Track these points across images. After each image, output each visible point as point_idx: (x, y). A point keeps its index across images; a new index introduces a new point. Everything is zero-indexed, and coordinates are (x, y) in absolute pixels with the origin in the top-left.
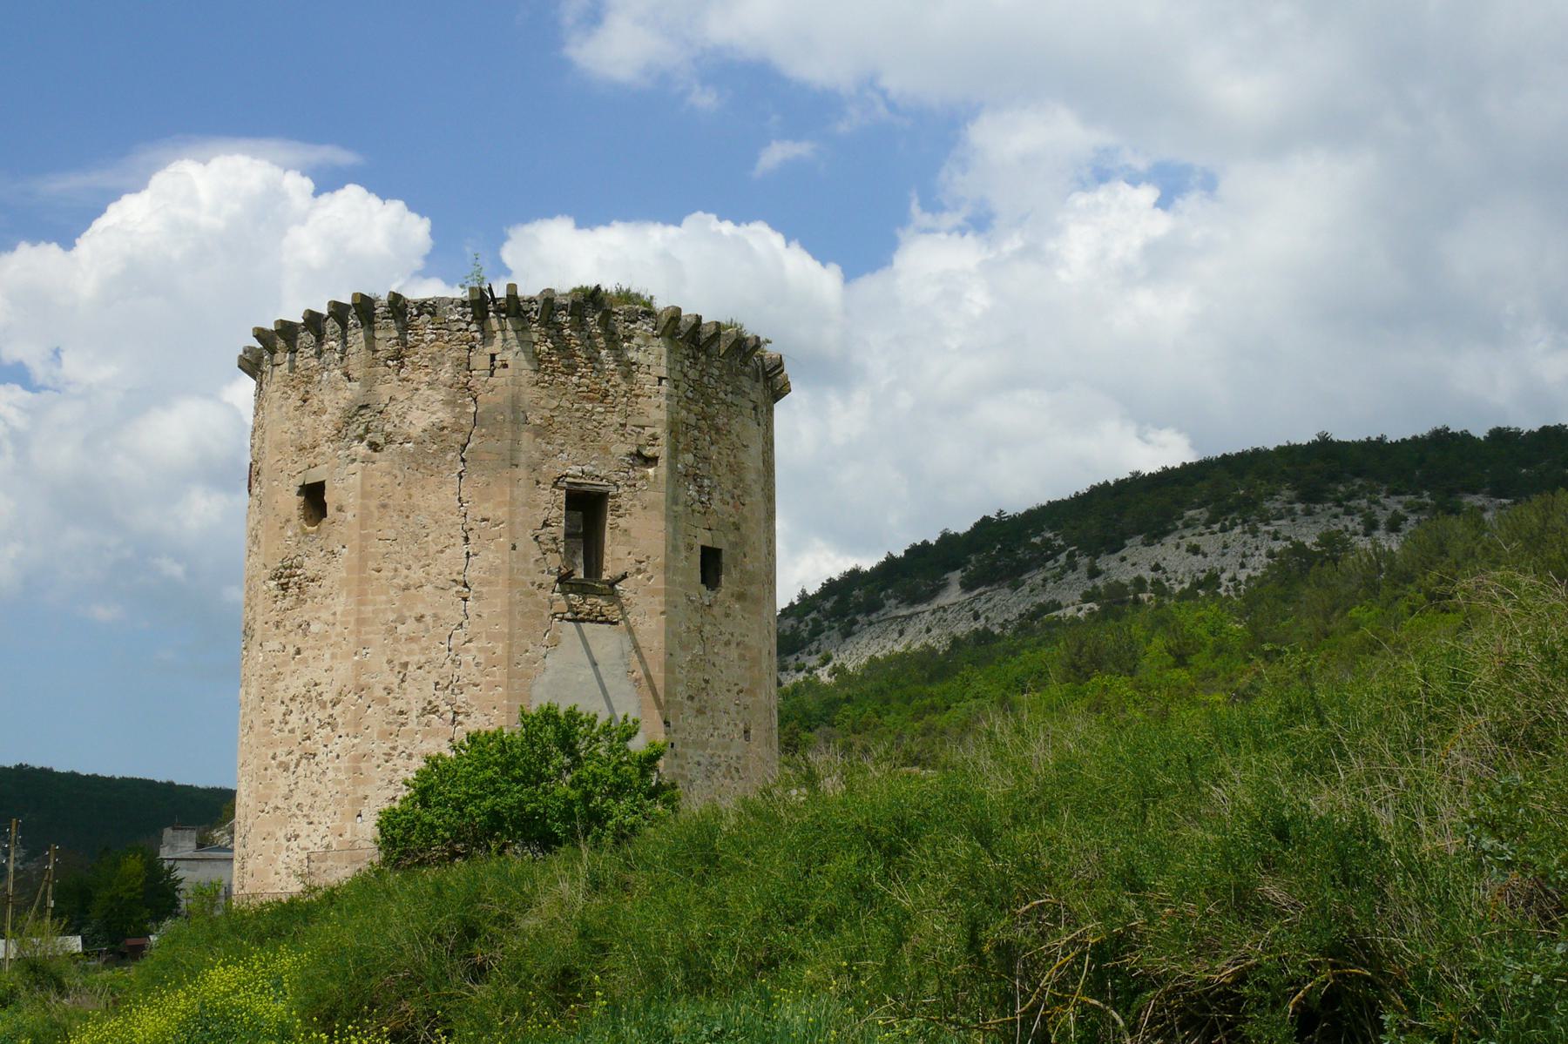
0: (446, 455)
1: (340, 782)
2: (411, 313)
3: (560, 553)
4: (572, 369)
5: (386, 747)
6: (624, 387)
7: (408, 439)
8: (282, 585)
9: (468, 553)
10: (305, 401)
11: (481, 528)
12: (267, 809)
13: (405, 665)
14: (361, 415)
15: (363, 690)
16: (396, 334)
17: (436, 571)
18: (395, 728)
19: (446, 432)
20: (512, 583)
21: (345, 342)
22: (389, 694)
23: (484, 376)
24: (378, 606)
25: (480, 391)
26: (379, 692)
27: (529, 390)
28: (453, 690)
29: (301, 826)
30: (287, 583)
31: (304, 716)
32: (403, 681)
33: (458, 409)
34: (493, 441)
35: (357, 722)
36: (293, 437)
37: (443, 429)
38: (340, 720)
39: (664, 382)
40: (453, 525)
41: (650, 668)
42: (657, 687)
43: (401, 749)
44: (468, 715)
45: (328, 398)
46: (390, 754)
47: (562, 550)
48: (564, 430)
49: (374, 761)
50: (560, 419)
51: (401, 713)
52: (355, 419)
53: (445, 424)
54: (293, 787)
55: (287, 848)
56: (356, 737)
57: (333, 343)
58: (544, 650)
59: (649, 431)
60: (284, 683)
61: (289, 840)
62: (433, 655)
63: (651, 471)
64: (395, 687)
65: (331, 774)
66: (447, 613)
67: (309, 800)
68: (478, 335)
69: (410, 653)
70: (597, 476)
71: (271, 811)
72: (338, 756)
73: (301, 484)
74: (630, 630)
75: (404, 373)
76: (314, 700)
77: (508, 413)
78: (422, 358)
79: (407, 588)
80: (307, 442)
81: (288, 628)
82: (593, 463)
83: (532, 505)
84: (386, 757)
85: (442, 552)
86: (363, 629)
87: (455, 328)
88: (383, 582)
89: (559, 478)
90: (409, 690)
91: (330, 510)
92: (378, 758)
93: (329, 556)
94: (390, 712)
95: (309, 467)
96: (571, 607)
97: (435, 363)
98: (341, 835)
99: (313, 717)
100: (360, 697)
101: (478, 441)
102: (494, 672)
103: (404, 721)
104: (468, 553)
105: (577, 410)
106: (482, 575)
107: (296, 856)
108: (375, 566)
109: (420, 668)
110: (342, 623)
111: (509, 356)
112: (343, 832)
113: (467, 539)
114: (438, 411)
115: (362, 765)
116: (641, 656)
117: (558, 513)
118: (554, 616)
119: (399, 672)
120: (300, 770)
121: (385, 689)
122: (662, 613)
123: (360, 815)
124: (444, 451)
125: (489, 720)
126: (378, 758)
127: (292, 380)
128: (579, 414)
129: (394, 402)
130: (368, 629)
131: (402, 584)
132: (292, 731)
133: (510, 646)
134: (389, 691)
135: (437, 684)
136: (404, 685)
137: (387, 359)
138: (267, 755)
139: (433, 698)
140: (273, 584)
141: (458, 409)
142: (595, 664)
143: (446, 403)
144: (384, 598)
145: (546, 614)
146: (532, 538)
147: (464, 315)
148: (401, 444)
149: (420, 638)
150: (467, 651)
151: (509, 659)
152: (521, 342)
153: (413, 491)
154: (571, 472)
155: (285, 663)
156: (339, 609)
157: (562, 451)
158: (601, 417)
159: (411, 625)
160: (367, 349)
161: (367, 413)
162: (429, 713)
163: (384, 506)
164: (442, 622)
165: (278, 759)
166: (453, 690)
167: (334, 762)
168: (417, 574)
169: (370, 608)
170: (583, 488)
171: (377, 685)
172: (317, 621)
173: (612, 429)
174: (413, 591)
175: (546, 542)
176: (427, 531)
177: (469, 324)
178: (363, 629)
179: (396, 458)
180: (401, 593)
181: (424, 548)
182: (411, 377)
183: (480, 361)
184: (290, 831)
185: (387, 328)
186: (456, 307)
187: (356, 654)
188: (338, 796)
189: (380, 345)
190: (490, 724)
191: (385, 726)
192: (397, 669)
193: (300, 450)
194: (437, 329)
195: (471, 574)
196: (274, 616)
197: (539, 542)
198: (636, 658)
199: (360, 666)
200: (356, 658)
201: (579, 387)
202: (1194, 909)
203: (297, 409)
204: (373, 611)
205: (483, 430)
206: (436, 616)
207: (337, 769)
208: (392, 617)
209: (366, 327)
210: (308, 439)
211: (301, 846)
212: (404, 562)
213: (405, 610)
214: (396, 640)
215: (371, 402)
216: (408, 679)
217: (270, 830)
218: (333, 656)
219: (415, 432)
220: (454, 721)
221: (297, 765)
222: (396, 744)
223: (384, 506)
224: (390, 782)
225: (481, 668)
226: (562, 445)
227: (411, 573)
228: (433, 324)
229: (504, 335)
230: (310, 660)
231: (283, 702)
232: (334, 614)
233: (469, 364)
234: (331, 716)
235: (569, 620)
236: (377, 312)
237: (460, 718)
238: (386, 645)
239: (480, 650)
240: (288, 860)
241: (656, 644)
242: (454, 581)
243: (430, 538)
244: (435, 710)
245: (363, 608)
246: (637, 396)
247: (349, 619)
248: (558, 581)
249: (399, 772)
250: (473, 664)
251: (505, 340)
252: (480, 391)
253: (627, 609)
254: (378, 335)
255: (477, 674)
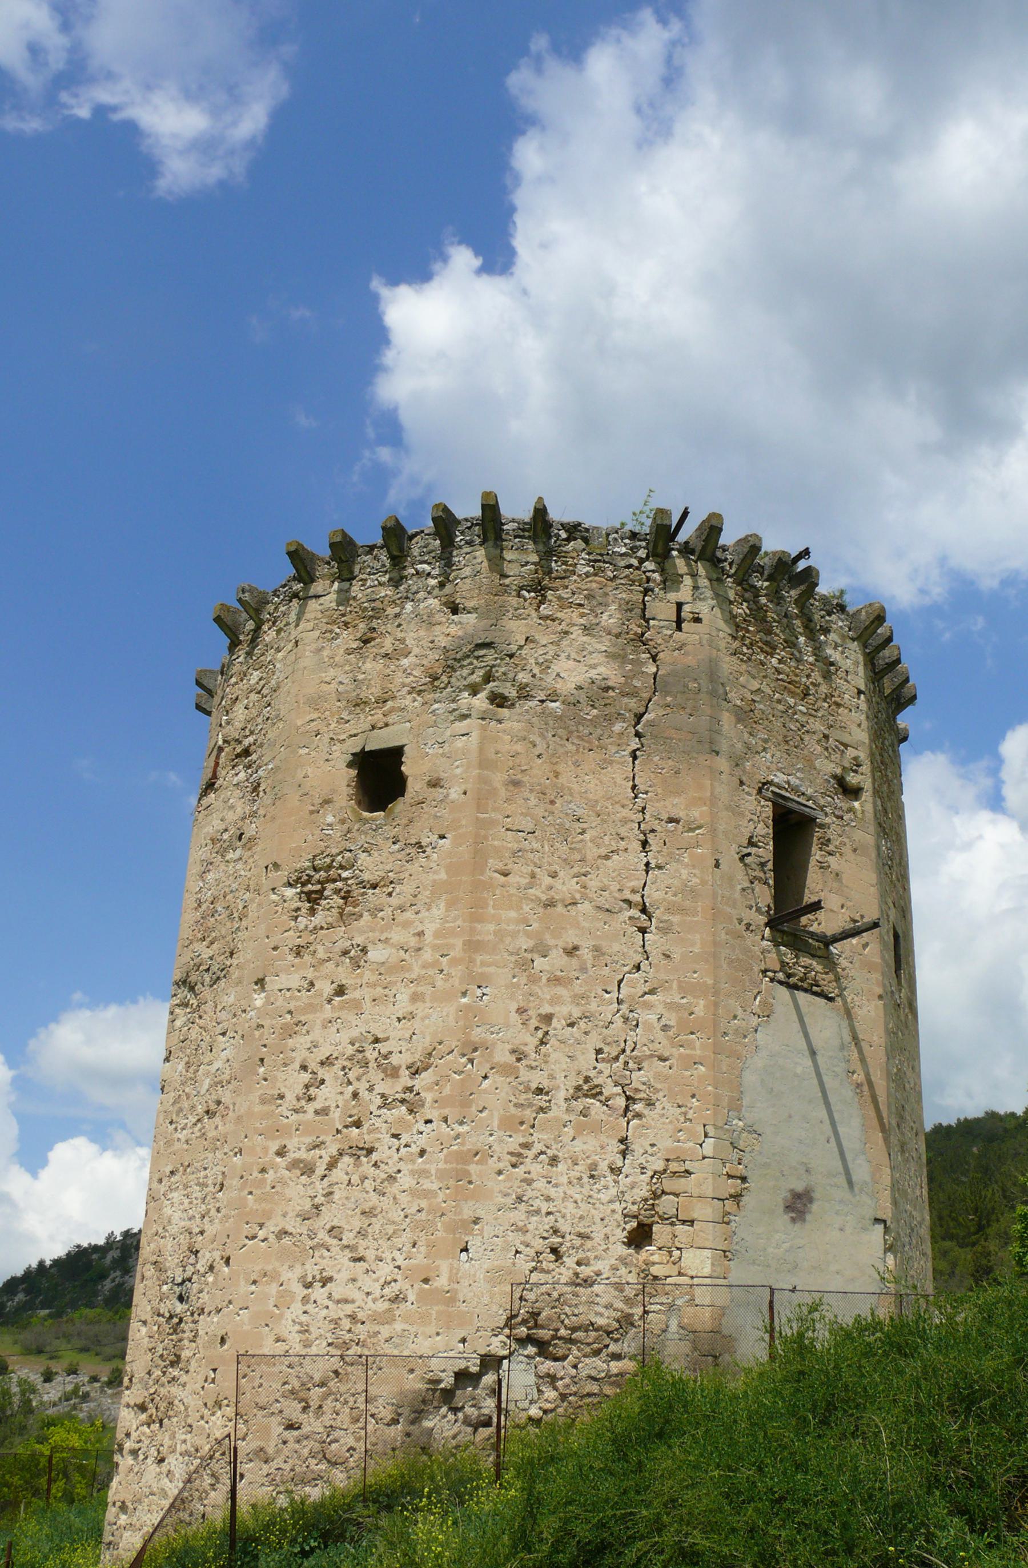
0: (612, 724)
1: (427, 1194)
2: (558, 536)
3: (769, 885)
4: (770, 649)
5: (513, 1143)
6: (824, 689)
7: (553, 697)
8: (309, 894)
9: (647, 864)
10: (366, 642)
11: (668, 831)
12: (261, 1234)
13: (548, 1018)
14: (477, 658)
15: (475, 1050)
16: (534, 558)
17: (599, 884)
18: (529, 1114)
19: (611, 693)
20: (716, 915)
21: (449, 564)
22: (519, 1060)
23: (667, 628)
24: (504, 926)
25: (662, 647)
26: (503, 1055)
27: (728, 659)
28: (626, 1063)
29: (340, 1265)
30: (321, 892)
31: (351, 1089)
32: (542, 1043)
33: (629, 667)
34: (683, 715)
35: (465, 1098)
36: (341, 688)
37: (607, 689)
38: (428, 1097)
39: (862, 696)
40: (625, 821)
41: (871, 1070)
42: (880, 1100)
43: (538, 1147)
44: (650, 1104)
45: (413, 636)
46: (520, 1155)
47: (771, 882)
48: (766, 722)
49: (493, 1164)
50: (762, 706)
51: (539, 1091)
52: (465, 663)
53: (610, 683)
54: (320, 1199)
55: (305, 1300)
56: (461, 1123)
57: (425, 566)
58: (755, 1021)
59: (851, 753)
60: (309, 1038)
61: (308, 1286)
62: (593, 1006)
63: (856, 804)
64: (530, 1049)
65: (406, 1181)
66: (616, 947)
67: (357, 1223)
68: (657, 576)
69: (555, 1000)
70: (803, 794)
71: (272, 1238)
72: (422, 1153)
73: (358, 750)
74: (848, 1014)
75: (544, 610)
76: (372, 1065)
77: (704, 682)
78: (573, 594)
79: (550, 904)
80: (372, 693)
81: (321, 954)
82: (798, 774)
83: (735, 810)
84: (514, 1159)
85: (607, 857)
86: (479, 958)
87: (622, 564)
88: (513, 891)
89: (764, 784)
90: (554, 1056)
91: (414, 786)
92: (499, 1159)
93: (413, 851)
94: (521, 1087)
95: (373, 727)
96: (783, 964)
97: (595, 603)
98: (426, 1281)
99: (371, 1089)
100: (471, 1061)
101: (661, 712)
102: (692, 1041)
103: (545, 1105)
104: (647, 864)
105: (779, 701)
106: (670, 897)
107: (325, 1312)
108: (500, 866)
109: (571, 1025)
110: (435, 948)
111: (704, 608)
112: (432, 1274)
113: (645, 844)
114: (600, 664)
115: (473, 1168)
116: (860, 1052)
117: (764, 830)
118: (764, 972)
119: (537, 1029)
120: (338, 1174)
121: (514, 1051)
122: (880, 997)
123: (465, 1250)
124: (609, 719)
125: (685, 1114)
126: (499, 1159)
127: (343, 615)
128: (780, 707)
129: (532, 645)
130: (487, 957)
131: (544, 897)
132: (323, 1112)
133: (716, 1005)
134: (520, 1056)
135: (599, 1051)
136: (543, 1048)
137: (521, 588)
138: (265, 1149)
139: (592, 1074)
140: (290, 892)
141: (629, 667)
142: (813, 1053)
143: (610, 655)
144: (513, 914)
145: (756, 969)
146: (737, 857)
147: (634, 549)
148: (542, 701)
149: (570, 981)
150: (649, 1006)
151: (716, 1024)
152: (717, 596)
153: (560, 768)
154: (776, 780)
155: (311, 1008)
156: (430, 929)
157: (765, 749)
158: (804, 719)
159: (556, 960)
160: (491, 570)
161: (490, 656)
162: (586, 1096)
163: (516, 784)
164: (609, 960)
165: (291, 1156)
166: (626, 1063)
167: (413, 1161)
168: (566, 886)
169: (491, 927)
170: (790, 804)
171: (500, 1046)
172: (380, 945)
173: (815, 737)
174: (560, 909)
175: (754, 866)
176: (585, 826)
177: (641, 561)
178: (479, 958)
179: (535, 720)
180: (541, 910)
181: (579, 851)
182: (559, 615)
183: (662, 608)
184: (311, 1270)
185: (521, 549)
186: (622, 539)
187: (464, 994)
188: (423, 1216)
189: (511, 570)
190: (687, 1120)
191: (513, 1110)
192: (534, 1023)
193: (357, 705)
194: (596, 561)
195: (653, 895)
196: (292, 939)
197: (746, 865)
198: (856, 1054)
199: (471, 1015)
200: (464, 1000)
201: (779, 673)
202: (779, 1427)
203: (349, 652)
204: (495, 933)
205: (669, 699)
206: (597, 949)
207: (421, 1174)
208: (525, 943)
209: (491, 543)
210: (373, 690)
211: (336, 1296)
212: (546, 867)
213: (547, 936)
214: (533, 980)
215: (496, 640)
216: (553, 1041)
217: (269, 1268)
218: (415, 998)
219: (566, 687)
220: (627, 1109)
221: (332, 1165)
222: (530, 1139)
223: (516, 784)
224: (520, 1199)
225: (671, 1033)
226: (766, 741)
227: (557, 884)
228: (589, 554)
229: (695, 581)
230: (367, 1005)
231: (304, 1068)
232: (421, 934)
233: (644, 610)
234: (410, 1089)
235: (781, 983)
236: (505, 527)
237: (638, 1107)
238: (517, 986)
239: (670, 1006)
240: (304, 1318)
241: (875, 1038)
242: (626, 901)
243: (587, 836)
244: (595, 1093)
245: (478, 926)
246: (838, 705)
247: (452, 941)
248: (767, 925)
249: (535, 1185)
250: (658, 1026)
251: (696, 588)
252: (662, 647)
253: (844, 982)
254: (508, 555)
255: (665, 1042)
